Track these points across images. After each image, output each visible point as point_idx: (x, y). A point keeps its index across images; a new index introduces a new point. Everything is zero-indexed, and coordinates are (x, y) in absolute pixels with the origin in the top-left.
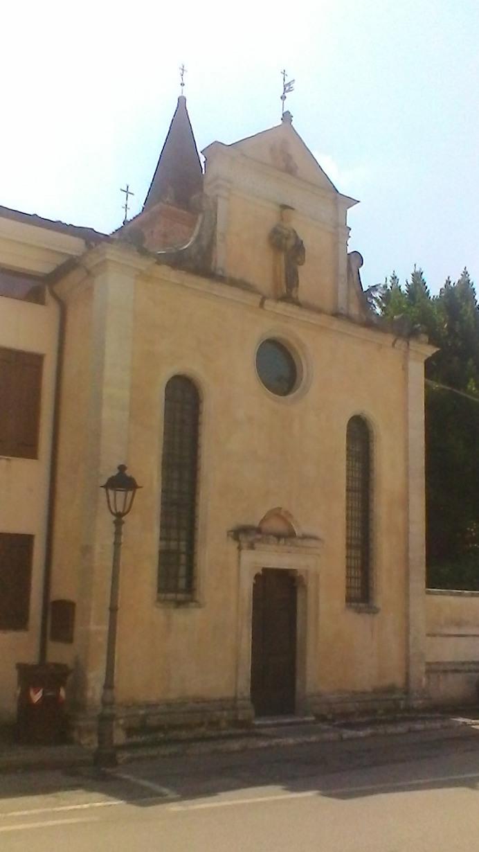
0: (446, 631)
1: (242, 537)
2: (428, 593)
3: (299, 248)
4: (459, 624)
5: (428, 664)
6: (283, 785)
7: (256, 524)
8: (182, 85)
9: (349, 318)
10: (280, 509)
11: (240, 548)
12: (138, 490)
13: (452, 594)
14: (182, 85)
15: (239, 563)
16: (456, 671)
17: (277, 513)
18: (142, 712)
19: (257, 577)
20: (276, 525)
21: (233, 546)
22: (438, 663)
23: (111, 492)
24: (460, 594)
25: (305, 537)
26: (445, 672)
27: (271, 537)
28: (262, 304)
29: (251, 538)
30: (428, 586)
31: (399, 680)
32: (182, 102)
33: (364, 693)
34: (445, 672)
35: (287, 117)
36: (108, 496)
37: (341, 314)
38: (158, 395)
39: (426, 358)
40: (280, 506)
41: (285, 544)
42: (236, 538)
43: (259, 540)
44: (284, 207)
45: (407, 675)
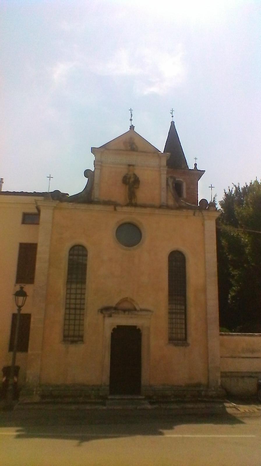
0: (244, 355)
1: (104, 312)
2: (221, 335)
3: (137, 181)
4: (253, 351)
5: (221, 372)
6: (17, 426)
7: (114, 305)
8: (173, 117)
9: (168, 207)
10: (127, 298)
11: (104, 317)
12: (27, 297)
13: (245, 335)
14: (131, 120)
15: (104, 324)
16: (251, 377)
17: (125, 300)
18: (51, 389)
19: (114, 330)
20: (126, 305)
21: (101, 316)
22: (238, 372)
23: (17, 297)
24: (252, 335)
25: (141, 310)
26: (243, 377)
27: (120, 311)
28: (115, 209)
29: (109, 312)
30: (220, 331)
31: (204, 381)
32: (173, 123)
33: (181, 386)
34: (243, 377)
35: (132, 127)
36: (16, 298)
37: (163, 206)
38: (65, 254)
39: (216, 218)
40: (127, 297)
41: (128, 314)
42: (102, 312)
43: (113, 313)
44: (129, 165)
45: (208, 379)
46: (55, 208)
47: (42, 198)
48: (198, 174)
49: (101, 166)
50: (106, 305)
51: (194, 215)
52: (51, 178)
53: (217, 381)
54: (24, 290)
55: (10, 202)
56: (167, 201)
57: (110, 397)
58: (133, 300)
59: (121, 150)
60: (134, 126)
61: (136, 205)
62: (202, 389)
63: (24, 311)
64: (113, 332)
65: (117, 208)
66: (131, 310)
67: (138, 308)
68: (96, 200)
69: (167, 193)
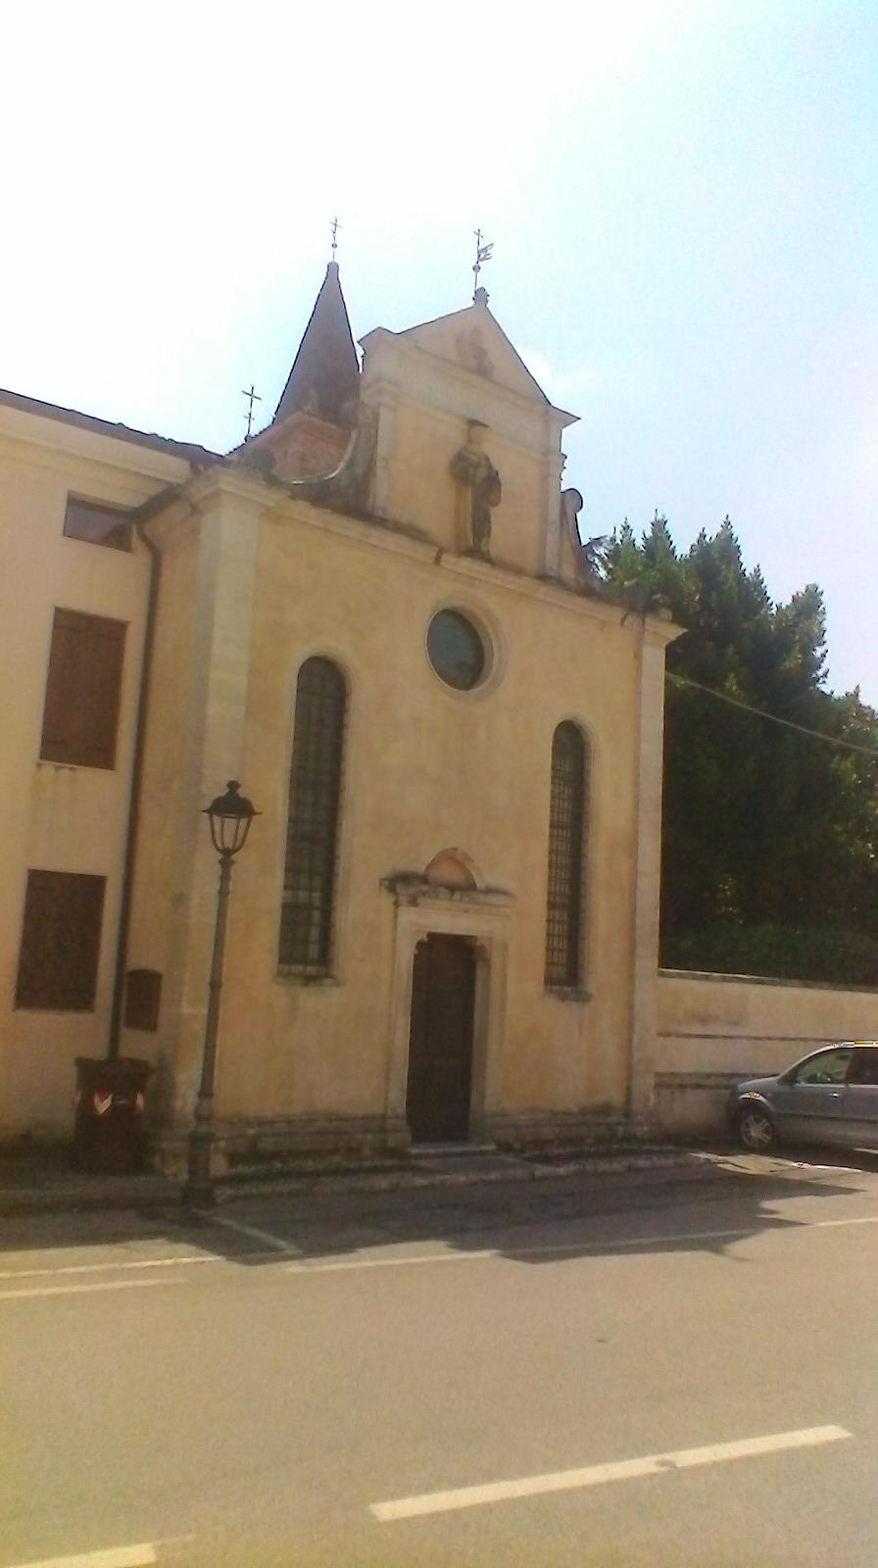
0: (685, 1029)
1: (399, 887)
2: (662, 975)
3: (493, 482)
4: (704, 1020)
5: (658, 1075)
7: (421, 869)
9: (560, 583)
10: (456, 849)
11: (397, 904)
15: (395, 925)
16: (699, 1086)
17: (450, 856)
18: (251, 1132)
19: (420, 945)
20: (449, 873)
21: (387, 901)
22: (672, 1074)
23: (217, 820)
24: (707, 978)
25: (489, 891)
26: (683, 1087)
27: (442, 889)
28: (438, 560)
29: (413, 890)
30: (661, 965)
31: (616, 1096)
32: (333, 270)
33: (567, 1113)
34: (683, 1087)
35: (481, 296)
37: (550, 577)
39: (667, 642)
41: (461, 900)
42: (392, 889)
43: (424, 894)
50: (403, 866)
51: (623, 621)
52: (254, 399)
53: (647, 1099)
56: (559, 566)
57: (414, 1151)
58: (467, 858)
60: (473, 295)
61: (487, 559)
62: (614, 1119)
64: (416, 952)
65: (444, 557)
66: (465, 889)
68: (380, 513)
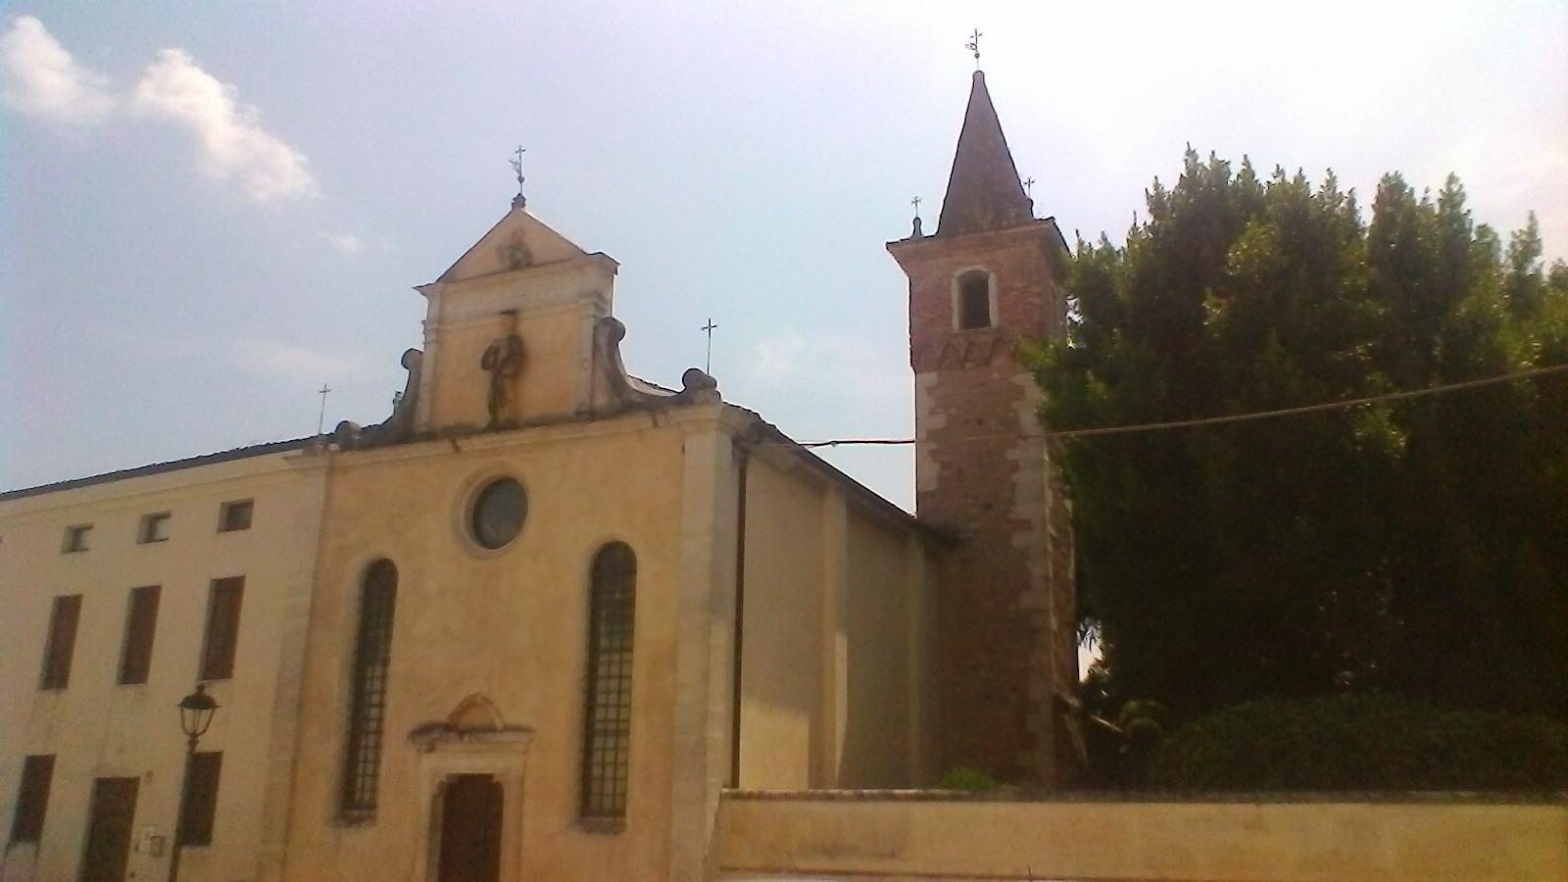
0: (802, 864)
7: (443, 718)
8: (977, 56)
10: (475, 695)
12: (217, 710)
28: (457, 449)
32: (979, 79)
35: (519, 201)
46: (331, 471)
47: (299, 452)
48: (908, 252)
49: (438, 331)
50: (426, 718)
54: (207, 692)
55: (229, 477)
59: (493, 274)
63: (205, 745)
67: (499, 724)
69: (593, 372)
